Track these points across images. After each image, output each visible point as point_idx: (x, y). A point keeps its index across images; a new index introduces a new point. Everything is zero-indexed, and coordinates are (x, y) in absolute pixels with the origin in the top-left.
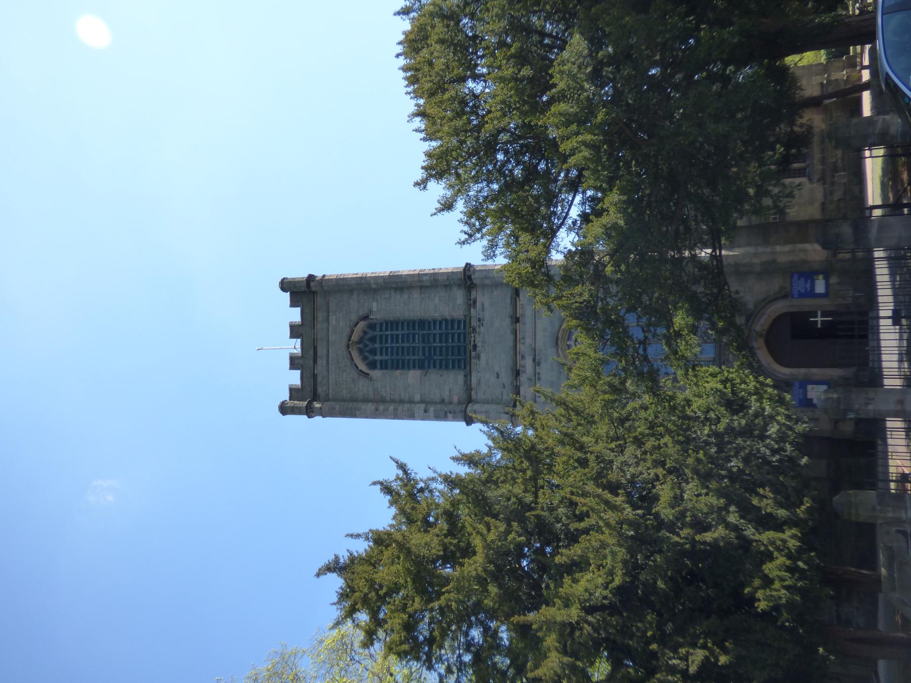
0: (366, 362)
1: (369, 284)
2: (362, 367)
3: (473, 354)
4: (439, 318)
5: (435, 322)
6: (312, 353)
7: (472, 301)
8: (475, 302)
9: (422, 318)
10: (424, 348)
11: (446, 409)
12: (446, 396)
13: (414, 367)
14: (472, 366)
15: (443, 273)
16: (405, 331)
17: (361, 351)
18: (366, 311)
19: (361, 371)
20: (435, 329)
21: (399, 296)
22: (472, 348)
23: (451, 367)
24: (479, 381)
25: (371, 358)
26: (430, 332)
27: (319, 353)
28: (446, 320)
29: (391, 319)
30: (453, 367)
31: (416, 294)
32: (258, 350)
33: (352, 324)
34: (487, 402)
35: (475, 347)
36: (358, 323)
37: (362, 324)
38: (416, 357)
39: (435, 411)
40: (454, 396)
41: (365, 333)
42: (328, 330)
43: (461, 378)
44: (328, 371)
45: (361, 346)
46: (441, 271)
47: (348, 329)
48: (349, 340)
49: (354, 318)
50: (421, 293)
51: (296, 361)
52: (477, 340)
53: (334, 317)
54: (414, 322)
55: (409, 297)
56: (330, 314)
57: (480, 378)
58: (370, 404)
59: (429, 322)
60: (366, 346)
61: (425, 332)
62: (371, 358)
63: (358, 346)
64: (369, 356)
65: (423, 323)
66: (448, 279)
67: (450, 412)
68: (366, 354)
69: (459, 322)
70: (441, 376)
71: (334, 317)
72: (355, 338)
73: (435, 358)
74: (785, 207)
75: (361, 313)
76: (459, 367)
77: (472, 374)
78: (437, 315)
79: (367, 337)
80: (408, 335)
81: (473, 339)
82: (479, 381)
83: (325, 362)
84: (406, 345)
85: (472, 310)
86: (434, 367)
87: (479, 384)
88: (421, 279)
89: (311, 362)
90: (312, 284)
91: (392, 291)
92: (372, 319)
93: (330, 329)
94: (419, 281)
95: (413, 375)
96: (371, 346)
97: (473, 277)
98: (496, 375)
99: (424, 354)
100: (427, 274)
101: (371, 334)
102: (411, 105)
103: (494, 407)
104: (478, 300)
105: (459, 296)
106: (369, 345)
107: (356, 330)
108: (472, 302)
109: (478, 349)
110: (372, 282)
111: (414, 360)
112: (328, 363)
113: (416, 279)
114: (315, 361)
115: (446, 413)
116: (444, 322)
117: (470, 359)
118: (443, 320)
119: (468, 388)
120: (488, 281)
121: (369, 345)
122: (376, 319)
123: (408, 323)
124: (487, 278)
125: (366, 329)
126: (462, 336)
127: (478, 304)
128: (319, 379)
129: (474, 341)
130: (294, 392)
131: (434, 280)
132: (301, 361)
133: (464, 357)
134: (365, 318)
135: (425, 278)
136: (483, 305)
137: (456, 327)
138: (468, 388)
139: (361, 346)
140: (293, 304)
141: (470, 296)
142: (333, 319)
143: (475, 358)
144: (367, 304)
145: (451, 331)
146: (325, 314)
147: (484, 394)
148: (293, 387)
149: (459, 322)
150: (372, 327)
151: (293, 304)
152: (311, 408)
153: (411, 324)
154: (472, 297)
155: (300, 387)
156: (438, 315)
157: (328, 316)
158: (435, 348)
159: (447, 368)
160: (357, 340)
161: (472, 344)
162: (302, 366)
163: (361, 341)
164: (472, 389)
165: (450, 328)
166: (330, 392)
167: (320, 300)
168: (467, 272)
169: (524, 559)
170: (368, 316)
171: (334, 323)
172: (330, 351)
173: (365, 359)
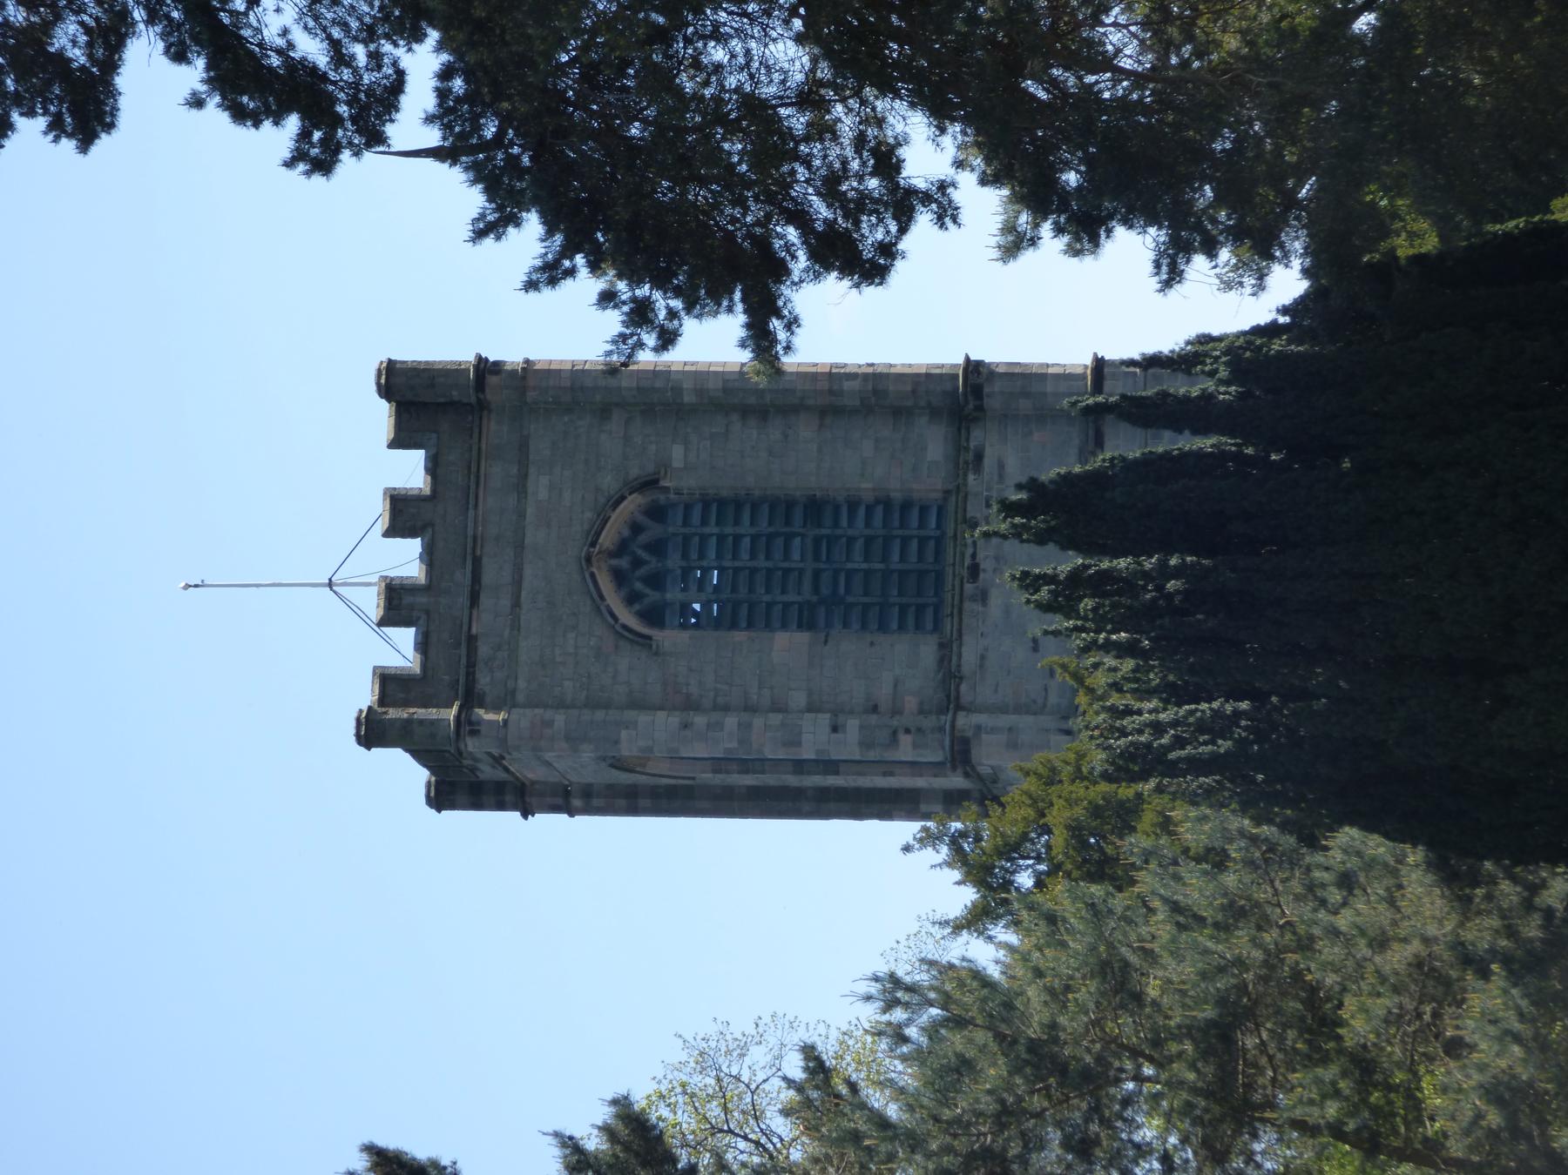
0: (637, 607)
1: (677, 390)
2: (627, 617)
3: (968, 587)
4: (868, 497)
5: (853, 505)
6: (464, 577)
7: (971, 454)
8: (979, 457)
9: (818, 494)
10: (817, 574)
11: (895, 723)
12: (884, 693)
13: (784, 626)
14: (966, 620)
15: (901, 377)
16: (763, 526)
17: (619, 577)
18: (651, 468)
19: (625, 627)
20: (851, 523)
21: (755, 432)
22: (965, 573)
23: (894, 625)
24: (983, 657)
25: (653, 596)
26: (839, 532)
27: (488, 577)
28: (887, 503)
29: (724, 493)
30: (902, 627)
31: (805, 430)
32: (187, 586)
33: (602, 500)
34: (1003, 709)
35: (975, 570)
36: (623, 498)
37: (634, 503)
38: (791, 597)
39: (861, 727)
40: (908, 698)
41: (636, 528)
42: (522, 515)
43: (928, 650)
44: (516, 626)
45: (624, 563)
46: (893, 370)
47: (589, 515)
48: (593, 544)
49: (609, 483)
50: (821, 426)
51: (407, 600)
52: (981, 555)
53: (544, 480)
54: (790, 504)
55: (786, 436)
56: (532, 470)
57: (986, 649)
58: (661, 715)
59: (837, 509)
60: (637, 563)
61: (824, 531)
62: (653, 596)
63: (614, 562)
64: (648, 591)
65: (815, 507)
66: (914, 392)
67: (907, 731)
68: (638, 586)
69: (924, 510)
70: (872, 644)
71: (544, 480)
72: (607, 539)
73: (850, 599)
74: (975, 920)
75: (634, 472)
76: (919, 627)
77: (966, 638)
78: (866, 487)
79: (643, 538)
80: (771, 537)
81: (970, 551)
82: (983, 657)
83: (505, 602)
84: (761, 562)
85: (971, 477)
86: (846, 625)
87: (981, 666)
88: (835, 387)
89: (463, 600)
90: (492, 380)
91: (735, 417)
92: (667, 489)
93: (530, 511)
94: (831, 392)
95: (787, 645)
96: (653, 564)
97: (986, 390)
98: (1031, 644)
99: (816, 589)
100: (852, 376)
101: (654, 531)
102: (446, 165)
103: (1030, 719)
104: (988, 452)
105: (934, 443)
106: (645, 563)
107: (614, 517)
108: (970, 456)
109: (982, 575)
110: (687, 385)
111: (786, 605)
112: (516, 604)
113: (825, 385)
114: (474, 599)
115: (895, 733)
116: (879, 510)
117: (961, 601)
118: (878, 501)
119: (950, 673)
120: (1025, 405)
121: (645, 563)
122: (678, 492)
123: (772, 508)
124: (1026, 394)
125: (641, 518)
126: (932, 544)
127: (989, 462)
128: (483, 650)
129: (974, 556)
130: (390, 684)
131: (875, 392)
132: (422, 599)
133: (935, 600)
134: (649, 484)
135: (847, 385)
136: (1001, 466)
137: (914, 522)
138: (950, 673)
139: (624, 563)
140: (401, 440)
141: (968, 440)
142: (540, 486)
143: (973, 599)
144: (653, 447)
145: (900, 532)
146: (514, 470)
147: (996, 691)
148: (386, 672)
149: (924, 510)
150: (656, 513)
151: (401, 440)
152: (470, 723)
153: (783, 506)
154: (972, 445)
155: (418, 670)
156: (869, 485)
157: (524, 476)
158: (850, 574)
159: (883, 627)
160: (612, 547)
161: (968, 562)
162: (428, 613)
163: (622, 548)
164: (961, 678)
165: (896, 523)
166: (522, 684)
167: (496, 430)
168: (970, 376)
169: (1163, 1099)
170: (656, 481)
171: (543, 494)
172: (528, 572)
173: (631, 599)
